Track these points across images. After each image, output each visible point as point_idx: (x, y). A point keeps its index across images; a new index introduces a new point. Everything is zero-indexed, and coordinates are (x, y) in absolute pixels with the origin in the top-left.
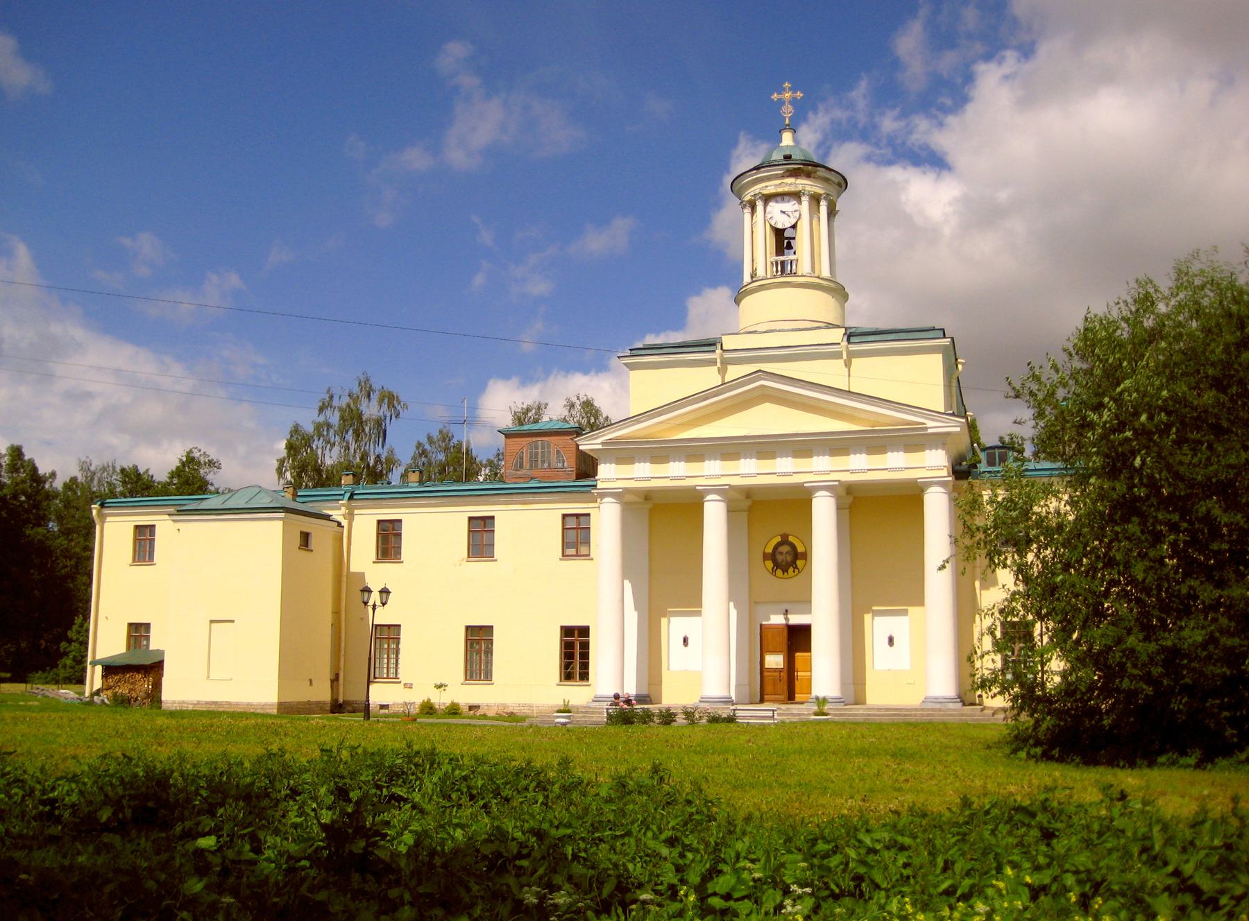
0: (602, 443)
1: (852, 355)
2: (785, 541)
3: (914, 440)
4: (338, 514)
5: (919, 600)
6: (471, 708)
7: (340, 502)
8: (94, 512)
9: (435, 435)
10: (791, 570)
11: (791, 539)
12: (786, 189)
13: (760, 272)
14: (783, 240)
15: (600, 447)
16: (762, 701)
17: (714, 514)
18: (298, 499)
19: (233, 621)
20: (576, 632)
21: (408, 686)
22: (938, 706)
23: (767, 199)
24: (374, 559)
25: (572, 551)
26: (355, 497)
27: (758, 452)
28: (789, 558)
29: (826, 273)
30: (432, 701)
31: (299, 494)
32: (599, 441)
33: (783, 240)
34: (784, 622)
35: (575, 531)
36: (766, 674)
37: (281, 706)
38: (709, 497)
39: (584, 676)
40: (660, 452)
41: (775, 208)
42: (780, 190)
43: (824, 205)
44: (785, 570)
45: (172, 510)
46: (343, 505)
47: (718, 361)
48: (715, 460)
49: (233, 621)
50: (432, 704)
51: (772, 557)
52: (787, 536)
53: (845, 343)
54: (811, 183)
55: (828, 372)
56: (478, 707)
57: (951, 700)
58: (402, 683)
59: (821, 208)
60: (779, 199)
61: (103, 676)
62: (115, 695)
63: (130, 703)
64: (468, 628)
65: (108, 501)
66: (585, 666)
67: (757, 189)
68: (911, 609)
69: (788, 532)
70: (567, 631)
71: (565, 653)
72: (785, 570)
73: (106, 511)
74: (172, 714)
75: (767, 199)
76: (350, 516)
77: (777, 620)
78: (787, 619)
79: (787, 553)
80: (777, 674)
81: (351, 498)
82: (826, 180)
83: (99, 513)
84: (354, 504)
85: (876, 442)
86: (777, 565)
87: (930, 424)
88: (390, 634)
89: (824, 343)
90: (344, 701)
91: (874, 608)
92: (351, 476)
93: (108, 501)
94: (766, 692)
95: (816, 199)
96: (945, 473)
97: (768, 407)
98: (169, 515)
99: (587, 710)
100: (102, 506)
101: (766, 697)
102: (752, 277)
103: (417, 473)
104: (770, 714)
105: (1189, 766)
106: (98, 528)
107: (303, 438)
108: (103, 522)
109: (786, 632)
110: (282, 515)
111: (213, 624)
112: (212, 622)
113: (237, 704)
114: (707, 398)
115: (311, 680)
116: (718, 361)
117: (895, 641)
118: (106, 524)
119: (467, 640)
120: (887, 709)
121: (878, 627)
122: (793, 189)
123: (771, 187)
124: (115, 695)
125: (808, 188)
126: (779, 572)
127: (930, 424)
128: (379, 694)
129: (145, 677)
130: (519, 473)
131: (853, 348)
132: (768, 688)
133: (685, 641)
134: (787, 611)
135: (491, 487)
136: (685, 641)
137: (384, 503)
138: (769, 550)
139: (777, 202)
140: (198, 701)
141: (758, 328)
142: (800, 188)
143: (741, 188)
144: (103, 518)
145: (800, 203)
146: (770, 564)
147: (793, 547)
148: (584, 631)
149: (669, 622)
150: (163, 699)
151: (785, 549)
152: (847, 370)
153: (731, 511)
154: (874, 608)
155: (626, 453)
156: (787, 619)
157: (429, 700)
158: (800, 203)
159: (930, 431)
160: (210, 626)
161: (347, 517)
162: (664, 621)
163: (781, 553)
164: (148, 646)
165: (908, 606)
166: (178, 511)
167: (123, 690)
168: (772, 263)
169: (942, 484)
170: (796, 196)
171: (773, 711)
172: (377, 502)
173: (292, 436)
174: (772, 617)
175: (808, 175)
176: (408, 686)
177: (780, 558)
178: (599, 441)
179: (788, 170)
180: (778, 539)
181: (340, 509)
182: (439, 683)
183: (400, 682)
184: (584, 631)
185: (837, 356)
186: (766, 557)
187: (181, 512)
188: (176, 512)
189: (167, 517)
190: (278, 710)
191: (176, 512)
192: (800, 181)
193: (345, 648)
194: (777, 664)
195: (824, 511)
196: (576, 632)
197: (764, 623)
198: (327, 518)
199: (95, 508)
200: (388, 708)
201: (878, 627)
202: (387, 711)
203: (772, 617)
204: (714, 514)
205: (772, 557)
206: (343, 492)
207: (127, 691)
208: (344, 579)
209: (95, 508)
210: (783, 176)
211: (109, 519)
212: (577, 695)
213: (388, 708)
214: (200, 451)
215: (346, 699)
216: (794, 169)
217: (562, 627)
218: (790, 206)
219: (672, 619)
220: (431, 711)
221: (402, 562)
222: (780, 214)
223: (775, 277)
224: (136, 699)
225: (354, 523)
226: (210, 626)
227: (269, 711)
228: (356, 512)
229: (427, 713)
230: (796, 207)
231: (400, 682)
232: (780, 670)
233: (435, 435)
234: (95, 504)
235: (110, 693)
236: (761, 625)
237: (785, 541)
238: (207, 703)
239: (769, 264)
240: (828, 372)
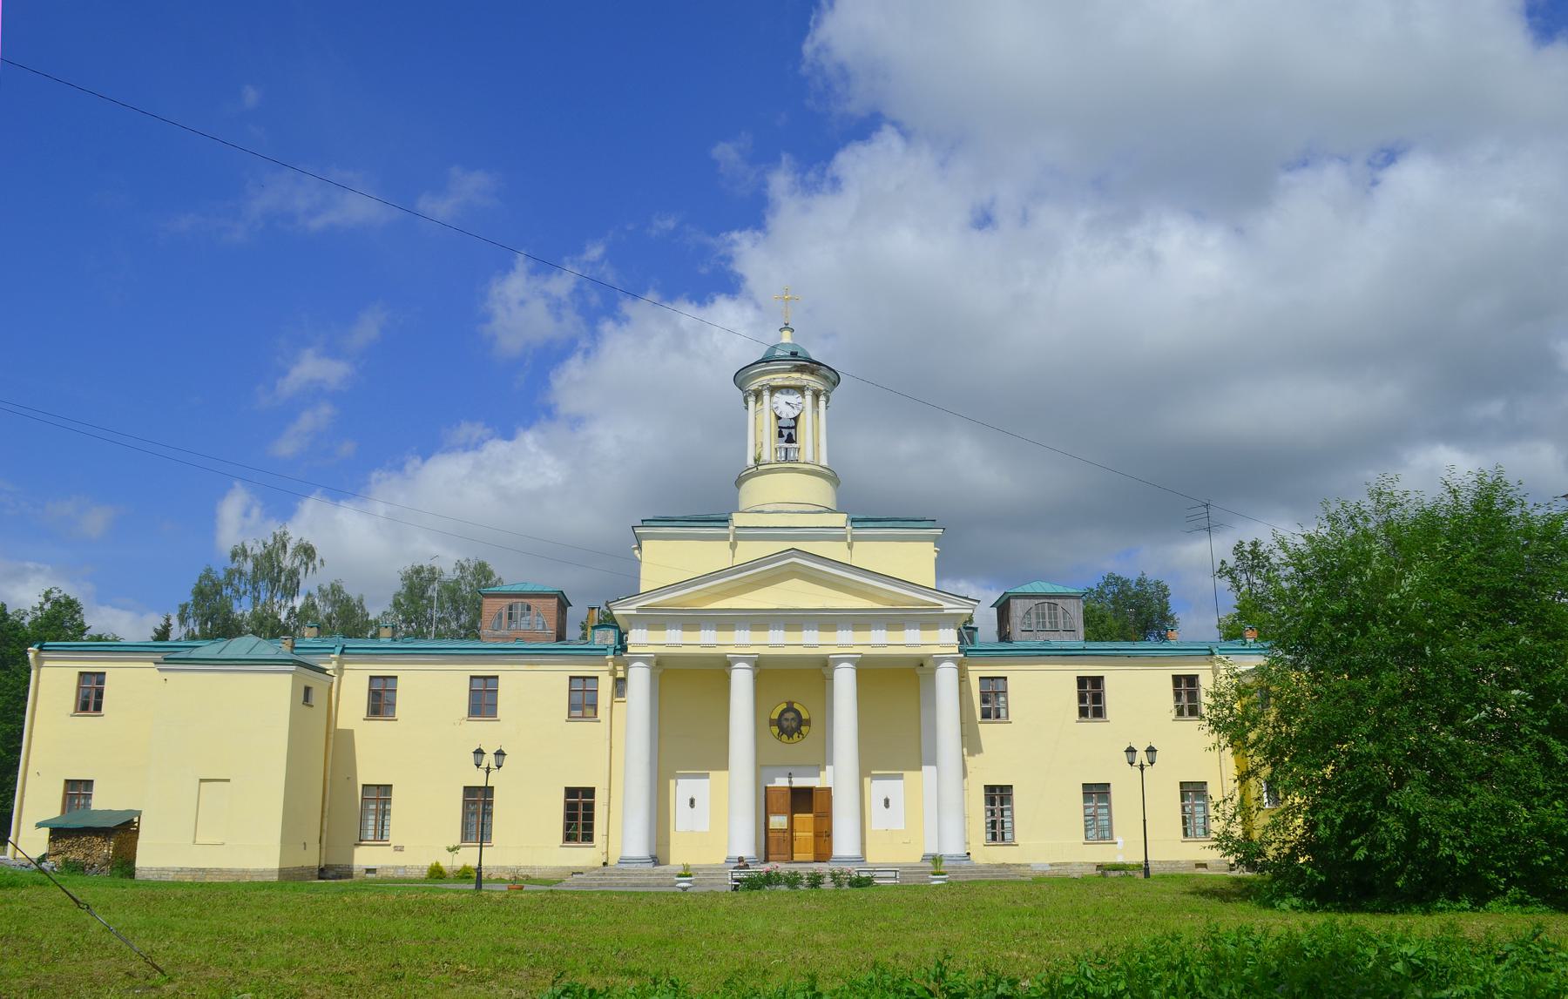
0: (637, 609)
1: (855, 538)
2: (790, 708)
3: (929, 620)
4: (331, 667)
5: (723, 764)
6: (368, 871)
7: (332, 656)
8: (31, 656)
9: (327, 587)
10: (796, 735)
11: (796, 706)
12: (793, 383)
13: (766, 457)
14: (787, 433)
15: (635, 612)
16: (767, 860)
17: (742, 681)
18: (295, 651)
19: (228, 780)
20: (580, 794)
21: (399, 849)
22: (954, 864)
23: (774, 390)
24: (365, 716)
25: (578, 713)
26: (346, 651)
27: (717, 625)
28: (794, 724)
29: (824, 462)
30: (441, 864)
31: (296, 646)
32: (634, 607)
33: (787, 433)
34: (788, 785)
35: (581, 693)
36: (770, 835)
37: (281, 870)
38: (737, 665)
39: (588, 837)
40: (693, 620)
41: (781, 399)
42: (787, 383)
43: (822, 399)
44: (790, 736)
45: (159, 657)
46: (334, 659)
47: (849, 536)
48: (643, 629)
49: (228, 780)
50: (441, 868)
51: (778, 723)
52: (793, 703)
53: (849, 528)
54: (813, 379)
55: (836, 551)
56: (373, 871)
57: (640, 861)
58: (392, 846)
59: (750, 403)
60: (784, 391)
61: (50, 840)
62: (66, 861)
63: (84, 870)
64: (1084, 785)
65: (47, 644)
66: (589, 827)
67: (765, 380)
68: (907, 774)
69: (792, 700)
70: (571, 792)
71: (568, 814)
72: (790, 736)
73: (44, 655)
74: (148, 883)
75: (774, 390)
76: (340, 670)
77: (782, 782)
78: (790, 782)
79: (793, 719)
80: (781, 835)
81: (342, 652)
82: (826, 378)
83: (36, 656)
84: (345, 658)
85: (895, 619)
86: (783, 731)
87: (946, 605)
88: (380, 794)
89: (828, 526)
90: (326, 865)
91: (873, 772)
92: (316, 629)
93: (47, 644)
94: (771, 852)
95: (816, 395)
96: (956, 650)
97: (796, 584)
98: (156, 663)
99: (711, 871)
100: (41, 649)
101: (770, 857)
102: (755, 460)
103: (390, 629)
104: (893, 874)
105: (1464, 909)
106: (33, 673)
107: (214, 585)
108: (39, 667)
109: (789, 794)
110: (293, 668)
111: (202, 784)
112: (201, 780)
113: (230, 871)
114: (741, 572)
115: (305, 844)
116: (849, 536)
117: (696, 803)
118: (42, 669)
119: (464, 801)
120: (912, 868)
121: (682, 789)
122: (798, 383)
123: (779, 379)
124: (66, 861)
125: (811, 384)
126: (785, 737)
127: (946, 605)
128: (365, 857)
129: (105, 841)
130: (497, 633)
131: (856, 532)
132: (773, 849)
133: (692, 802)
134: (790, 774)
135: (512, 647)
136: (692, 802)
137: (379, 658)
138: (775, 716)
139: (782, 393)
140: (181, 868)
141: (766, 508)
142: (805, 383)
143: (744, 379)
144: (40, 661)
145: (804, 397)
146: (776, 730)
147: (798, 713)
148: (590, 792)
149: (677, 784)
150: (137, 865)
151: (790, 715)
152: (731, 552)
153: (757, 679)
154: (873, 772)
155: (656, 619)
156: (790, 782)
157: (437, 863)
158: (804, 397)
159: (946, 611)
160: (200, 785)
161: (337, 671)
162: (672, 782)
163: (787, 720)
164: (87, 805)
165: (905, 770)
166: (165, 659)
167: (76, 855)
168: (776, 449)
169: (953, 660)
170: (801, 390)
171: (896, 871)
172: (467, 658)
173: (200, 581)
174: (777, 779)
175: (812, 373)
176: (399, 849)
177: (785, 724)
178: (634, 607)
179: (795, 366)
180: (784, 706)
181: (607, 665)
182: (451, 847)
183: (389, 845)
184: (590, 792)
185: (842, 538)
186: (772, 723)
187: (167, 660)
188: (162, 661)
189: (152, 665)
190: (279, 876)
191: (162, 661)
192: (804, 377)
193: (329, 809)
194: (780, 824)
195: (845, 682)
196: (580, 794)
197: (769, 785)
198: (323, 671)
199: (33, 651)
200: (375, 873)
201: (682, 789)
202: (374, 875)
203: (777, 779)
204: (742, 681)
205: (778, 723)
206: (333, 646)
207: (82, 857)
208: (332, 736)
209: (32, 652)
210: (790, 371)
211: (47, 663)
212: (582, 857)
213: (375, 873)
214: (60, 591)
215: (328, 863)
216: (802, 365)
217: (566, 788)
218: (794, 398)
219: (679, 780)
220: (441, 876)
221: (103, 715)
222: (784, 404)
223: (778, 462)
224: (93, 866)
225: (343, 678)
226: (200, 785)
227: (268, 879)
228: (346, 666)
229: (437, 878)
230: (800, 400)
231: (389, 845)
232: (784, 831)
233: (327, 587)
234: (32, 646)
235: (59, 859)
236: (766, 788)
237: (790, 708)
238: (1081, 864)
239: (773, 450)
240: (836, 551)
